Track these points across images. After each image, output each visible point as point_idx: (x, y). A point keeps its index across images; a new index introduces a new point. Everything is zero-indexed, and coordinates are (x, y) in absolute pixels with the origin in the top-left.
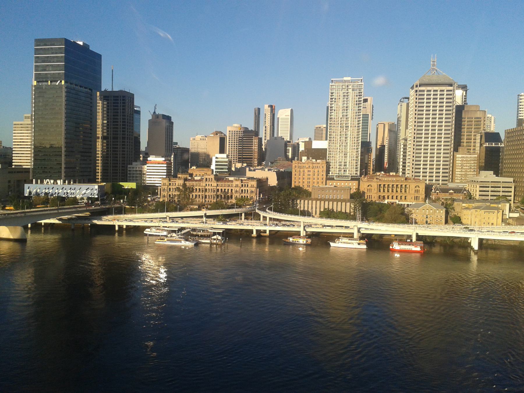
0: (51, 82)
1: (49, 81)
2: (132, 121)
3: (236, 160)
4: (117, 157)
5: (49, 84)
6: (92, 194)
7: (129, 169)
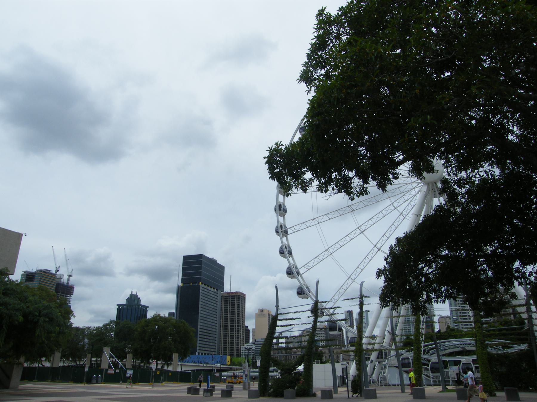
0: (192, 283)
5: (191, 285)
7: (242, 349)
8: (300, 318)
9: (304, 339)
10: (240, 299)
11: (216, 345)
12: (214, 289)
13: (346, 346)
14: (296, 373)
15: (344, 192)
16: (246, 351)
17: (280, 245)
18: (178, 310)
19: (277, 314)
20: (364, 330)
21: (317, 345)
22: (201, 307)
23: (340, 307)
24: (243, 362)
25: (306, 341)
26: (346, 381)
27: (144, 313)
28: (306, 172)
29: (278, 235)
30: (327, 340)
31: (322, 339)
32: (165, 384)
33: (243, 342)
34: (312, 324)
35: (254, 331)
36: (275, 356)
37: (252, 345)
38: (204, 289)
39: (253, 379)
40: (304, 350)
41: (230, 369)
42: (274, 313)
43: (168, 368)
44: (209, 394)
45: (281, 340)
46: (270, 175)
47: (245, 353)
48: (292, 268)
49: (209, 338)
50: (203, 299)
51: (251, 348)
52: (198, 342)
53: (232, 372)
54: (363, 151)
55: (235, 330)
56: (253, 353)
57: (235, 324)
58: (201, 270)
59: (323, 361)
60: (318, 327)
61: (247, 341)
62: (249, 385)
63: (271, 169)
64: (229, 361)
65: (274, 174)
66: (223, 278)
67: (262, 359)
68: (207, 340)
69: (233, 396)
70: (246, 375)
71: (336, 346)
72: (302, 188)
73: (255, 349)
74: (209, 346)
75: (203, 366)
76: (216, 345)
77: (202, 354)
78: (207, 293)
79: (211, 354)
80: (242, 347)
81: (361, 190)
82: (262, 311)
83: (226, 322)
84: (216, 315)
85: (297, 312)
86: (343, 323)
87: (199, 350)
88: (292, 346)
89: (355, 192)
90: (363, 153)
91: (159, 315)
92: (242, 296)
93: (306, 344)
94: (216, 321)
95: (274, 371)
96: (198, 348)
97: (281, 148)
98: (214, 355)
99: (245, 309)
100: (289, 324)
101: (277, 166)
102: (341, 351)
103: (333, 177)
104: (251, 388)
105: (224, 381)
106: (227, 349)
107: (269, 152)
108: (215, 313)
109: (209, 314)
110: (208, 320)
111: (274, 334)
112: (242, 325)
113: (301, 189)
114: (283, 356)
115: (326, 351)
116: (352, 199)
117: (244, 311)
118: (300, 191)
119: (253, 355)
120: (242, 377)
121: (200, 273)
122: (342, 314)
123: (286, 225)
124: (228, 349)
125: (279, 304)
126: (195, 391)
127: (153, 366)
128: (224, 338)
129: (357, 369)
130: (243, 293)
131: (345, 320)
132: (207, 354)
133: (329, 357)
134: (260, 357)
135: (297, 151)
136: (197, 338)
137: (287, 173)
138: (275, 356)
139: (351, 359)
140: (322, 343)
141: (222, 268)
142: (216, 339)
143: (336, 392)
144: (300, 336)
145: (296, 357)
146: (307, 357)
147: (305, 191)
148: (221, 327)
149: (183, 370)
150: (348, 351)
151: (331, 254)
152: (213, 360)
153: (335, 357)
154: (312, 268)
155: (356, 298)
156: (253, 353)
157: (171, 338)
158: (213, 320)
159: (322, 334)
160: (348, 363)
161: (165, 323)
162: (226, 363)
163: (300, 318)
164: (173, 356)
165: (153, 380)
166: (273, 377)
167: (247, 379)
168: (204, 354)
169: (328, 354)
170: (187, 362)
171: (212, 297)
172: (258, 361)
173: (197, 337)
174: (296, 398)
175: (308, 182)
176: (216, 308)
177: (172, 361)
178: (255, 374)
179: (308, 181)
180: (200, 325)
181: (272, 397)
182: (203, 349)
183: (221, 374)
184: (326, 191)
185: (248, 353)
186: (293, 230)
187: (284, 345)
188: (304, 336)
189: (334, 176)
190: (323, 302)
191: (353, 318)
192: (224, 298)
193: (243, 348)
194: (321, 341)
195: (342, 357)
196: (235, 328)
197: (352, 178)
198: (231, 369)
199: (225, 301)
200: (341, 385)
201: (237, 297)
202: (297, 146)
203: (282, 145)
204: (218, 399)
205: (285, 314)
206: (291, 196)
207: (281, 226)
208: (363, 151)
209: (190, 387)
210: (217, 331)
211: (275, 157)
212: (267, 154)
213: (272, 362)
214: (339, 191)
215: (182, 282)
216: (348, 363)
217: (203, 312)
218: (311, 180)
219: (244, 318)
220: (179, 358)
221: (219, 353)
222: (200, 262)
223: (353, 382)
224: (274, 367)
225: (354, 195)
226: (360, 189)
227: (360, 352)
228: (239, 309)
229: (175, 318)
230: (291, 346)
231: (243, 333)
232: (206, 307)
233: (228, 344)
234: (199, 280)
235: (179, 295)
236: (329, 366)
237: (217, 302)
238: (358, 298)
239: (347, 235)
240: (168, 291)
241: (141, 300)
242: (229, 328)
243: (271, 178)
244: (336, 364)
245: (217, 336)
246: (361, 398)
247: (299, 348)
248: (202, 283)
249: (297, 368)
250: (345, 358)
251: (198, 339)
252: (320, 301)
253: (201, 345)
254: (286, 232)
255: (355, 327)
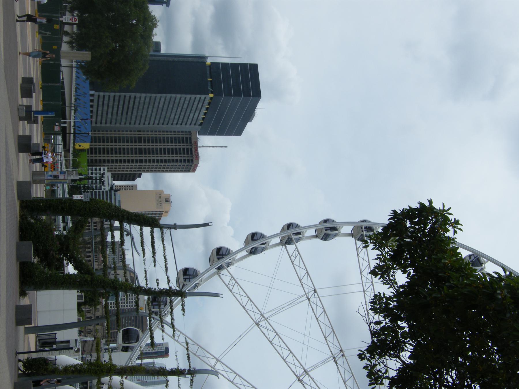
0: (211, 81)
1: (211, 79)
2: (181, 171)
4: (116, 153)
5: (208, 79)
6: (79, 85)
7: (102, 168)
9: (121, 272)
10: (186, 164)
11: (108, 125)
12: (203, 119)
13: (106, 347)
14: (61, 261)
16: (98, 175)
18: (165, 58)
19: (161, 227)
20: (135, 378)
21: (109, 295)
22: (171, 97)
24: (80, 170)
25: (115, 277)
26: (47, 349)
28: (406, 275)
29: (283, 230)
30: (118, 313)
31: (120, 305)
32: (36, 39)
33: (113, 170)
34: (145, 286)
35: (133, 188)
36: (90, 224)
37: (110, 186)
40: (101, 273)
41: (67, 148)
42: (163, 221)
43: (66, 42)
44: (24, 114)
45: (117, 234)
46: (399, 212)
47: (96, 174)
49: (120, 112)
50: (185, 100)
52: (112, 94)
53: (63, 153)
54: (450, 379)
56: (96, 187)
57: (143, 157)
59: (83, 307)
60: (140, 297)
61: (116, 177)
62: (41, 182)
63: (409, 213)
64: (81, 148)
65: (401, 219)
66: (221, 133)
67: (86, 202)
68: (115, 109)
70: (58, 176)
71: (108, 330)
72: (378, 267)
73: (103, 190)
74: (105, 112)
75: (71, 103)
77: (92, 101)
79: (92, 117)
80: (106, 168)
81: (377, 373)
82: (167, 200)
83: (147, 140)
84: (158, 124)
85: (166, 260)
86: (147, 340)
87: (99, 96)
88: (108, 252)
89: (373, 362)
90: (447, 380)
91: (155, 26)
92: (191, 166)
93: (112, 277)
94: (149, 124)
95: (65, 224)
96: (102, 94)
97: (449, 231)
98: (91, 121)
99: (170, 171)
100: (145, 248)
101: (416, 224)
102: (98, 338)
103: (399, 323)
104: (34, 185)
105: (47, 140)
106: (101, 144)
107: (442, 208)
108: (161, 122)
109: (159, 112)
110: (150, 110)
111: (127, 223)
113: (376, 265)
114: (91, 238)
115: (100, 311)
116: (361, 357)
117: (167, 171)
118: (374, 263)
119: (93, 186)
120: (54, 169)
121: (228, 94)
122: (163, 339)
125: (179, 230)
126: (27, 92)
127: (67, 18)
128: (119, 137)
129: (66, 367)
131: (152, 344)
132: (91, 109)
133: (88, 318)
134: (89, 200)
135: (444, 258)
138: (90, 224)
140: (112, 305)
141: (239, 132)
142: (118, 125)
143: (28, 331)
144: (125, 267)
145: (90, 261)
146: (89, 279)
149: (62, 69)
150: (98, 350)
152: (82, 120)
153: (90, 328)
155: (190, 363)
156: (96, 187)
157: (116, 47)
159: (128, 304)
160: (78, 351)
161: (142, 36)
162: (78, 142)
164: (86, 51)
166: (55, 222)
167: (50, 178)
169: (94, 315)
170: (77, 77)
171: (189, 115)
172: (82, 195)
173: (120, 91)
174: (18, 262)
175: (389, 278)
177: (77, 50)
178: (60, 191)
179: (391, 278)
180: (140, 97)
181: (20, 222)
182: (101, 103)
183: (59, 134)
184: (374, 309)
185: (96, 179)
186: (294, 255)
187: (109, 239)
188: (125, 273)
189: (402, 324)
190: (183, 305)
191: (156, 357)
192: (188, 136)
193: (104, 170)
194: (117, 303)
195: (88, 339)
196: (138, 157)
197: (398, 357)
198: (67, 150)
199: (183, 138)
200: (39, 340)
201: (190, 158)
202: (454, 259)
203: (455, 232)
204: (15, 129)
205: (163, 240)
207: (299, 233)
208: (450, 379)
209: (35, 81)
210: (132, 126)
211: (432, 220)
212: (437, 205)
213: (80, 221)
214: (373, 333)
216: (78, 351)
217: (163, 100)
218: (392, 283)
219: (155, 171)
220: (83, 62)
221: (94, 129)
222: (247, 94)
223: (45, 361)
224: (73, 223)
225: (369, 360)
226: (379, 371)
227: (96, 372)
228: (169, 162)
229: (152, 53)
230: (108, 251)
231: (129, 170)
233: (114, 146)
234: (218, 94)
235: (190, 59)
236: (73, 317)
237: (181, 124)
239: (291, 352)
240: (197, 41)
242: (137, 146)
243: (395, 212)
244: (76, 331)
245: (123, 125)
246: (17, 376)
247: (105, 265)
248: (211, 98)
249: (71, 263)
250: (87, 345)
251: (118, 94)
252: (185, 300)
253: (106, 99)
254: (288, 241)
255: (139, 362)
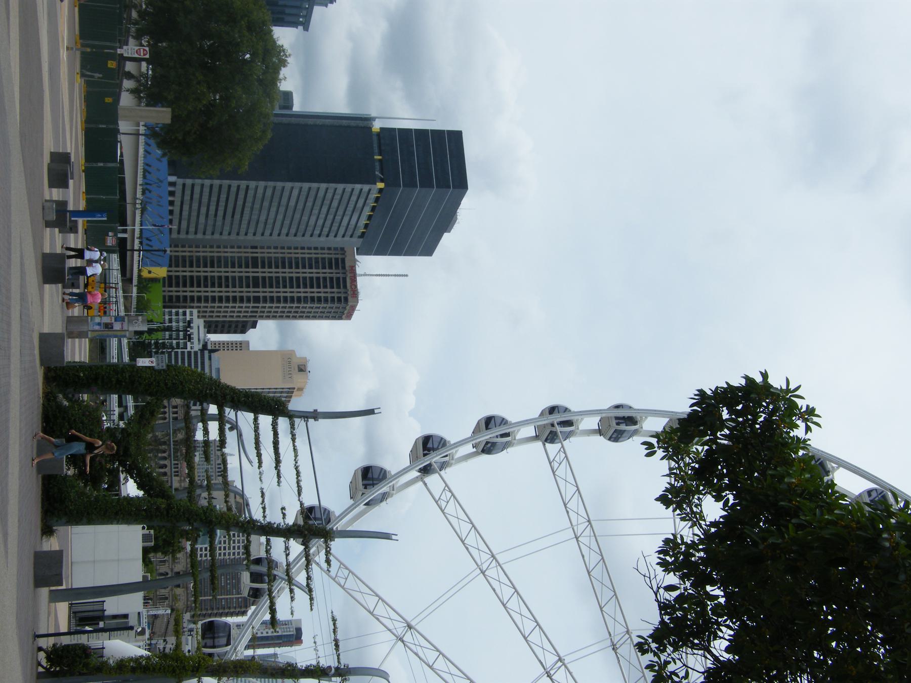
0: (380, 160)
1: (380, 157)
3: (234, 554)
5: (376, 157)
7: (188, 311)
8: (279, 482)
9: (219, 495)
10: (336, 305)
11: (200, 236)
12: (366, 226)
15: (662, 622)
16: (181, 324)
17: (512, 418)
21: (199, 536)
22: (310, 188)
23: (311, 605)
24: (149, 314)
26: (88, 628)
27: (288, 18)
28: (721, 504)
29: (542, 414)
31: (218, 552)
32: (77, 85)
34: (262, 519)
35: (241, 346)
36: (167, 410)
37: (202, 343)
38: (363, 196)
39: (100, 347)
40: (184, 496)
41: (128, 275)
42: (295, 405)
44: (53, 217)
45: (213, 427)
46: (709, 392)
47: (178, 321)
48: (443, 452)
49: (220, 213)
51: (190, 339)
52: (207, 182)
53: (120, 284)
55: (245, 289)
56: (178, 344)
57: (261, 292)
58: (421, 186)
59: (151, 555)
60: (253, 538)
61: (212, 327)
62: (81, 335)
63: (727, 395)
64: (152, 275)
65: (712, 404)
67: (159, 371)
68: (213, 208)
69: (47, 286)
70: (111, 324)
71: (195, 595)
72: (671, 489)
73: (189, 349)
74: (194, 214)
75: (135, 198)
76: (200, 236)
77: (172, 194)
78: (351, 206)
79: (171, 222)
82: (302, 369)
83: (268, 263)
84: (287, 235)
88: (197, 459)
89: (663, 657)
91: (283, 63)
92: (345, 308)
94: (271, 235)
95: (122, 409)
96: (189, 182)
97: (797, 426)
99: (308, 318)
101: (739, 414)
102: (178, 611)
103: (708, 588)
107: (784, 387)
108: (293, 231)
109: (290, 213)
110: (273, 209)
111: (231, 407)
112: (259, 310)
113: (668, 486)
115: (182, 563)
120: (105, 313)
121: (411, 184)
122: (292, 614)
123: (571, 439)
124: (186, 272)
125: (321, 421)
126: (59, 178)
127: (130, 49)
129: (122, 660)
130: (356, 313)
131: (273, 622)
132: (171, 208)
133: (161, 574)
135: (789, 475)
136: (219, 178)
137: (717, 444)
138: (167, 410)
139: (153, 642)
140: (204, 552)
141: (429, 251)
142: (217, 236)
143: (56, 597)
144: (226, 485)
145: (165, 474)
146: (163, 506)
147: (664, 500)
148: (252, 247)
149: (121, 138)
151: (483, 572)
154: (443, 511)
156: (178, 344)
157: (215, 99)
158: (274, 222)
159: (232, 551)
160: (143, 632)
161: (261, 82)
162: (147, 265)
163: (279, 482)
164: (163, 106)
165: (89, 50)
167: (97, 328)
168: (171, 198)
169: (172, 570)
170: (146, 151)
172: (153, 359)
175: (691, 509)
176: (308, 233)
178: (114, 352)
179: (695, 509)
180: (257, 187)
182: (187, 198)
183: (113, 252)
184: (663, 564)
185: (178, 331)
186: (443, 497)
190: (328, 553)
191: (280, 645)
192: (340, 256)
195: (160, 612)
196: (251, 292)
197: (707, 649)
199: (330, 259)
201: (343, 296)
203: (808, 429)
204: (38, 241)
206: (648, 455)
207: (569, 423)
209: (73, 160)
211: (767, 407)
212: (777, 382)
213: (148, 403)
214: (664, 607)
215: (381, 129)
217: (295, 193)
221: (174, 244)
222: (443, 184)
223: (85, 651)
224: (136, 407)
225: (655, 654)
227: (174, 671)
230: (198, 458)
232: (309, 204)
233: (209, 272)
234: (391, 181)
236: (135, 572)
237: (327, 236)
238: (339, 662)
240: (357, 89)
241: (326, 6)
242: (251, 272)
243: (702, 393)
244: (139, 597)
245: (225, 237)
247: (192, 482)
248: (381, 191)
249: (132, 477)
250: (158, 622)
251: (217, 182)
253: (197, 190)
254: (552, 438)
255: (250, 652)
